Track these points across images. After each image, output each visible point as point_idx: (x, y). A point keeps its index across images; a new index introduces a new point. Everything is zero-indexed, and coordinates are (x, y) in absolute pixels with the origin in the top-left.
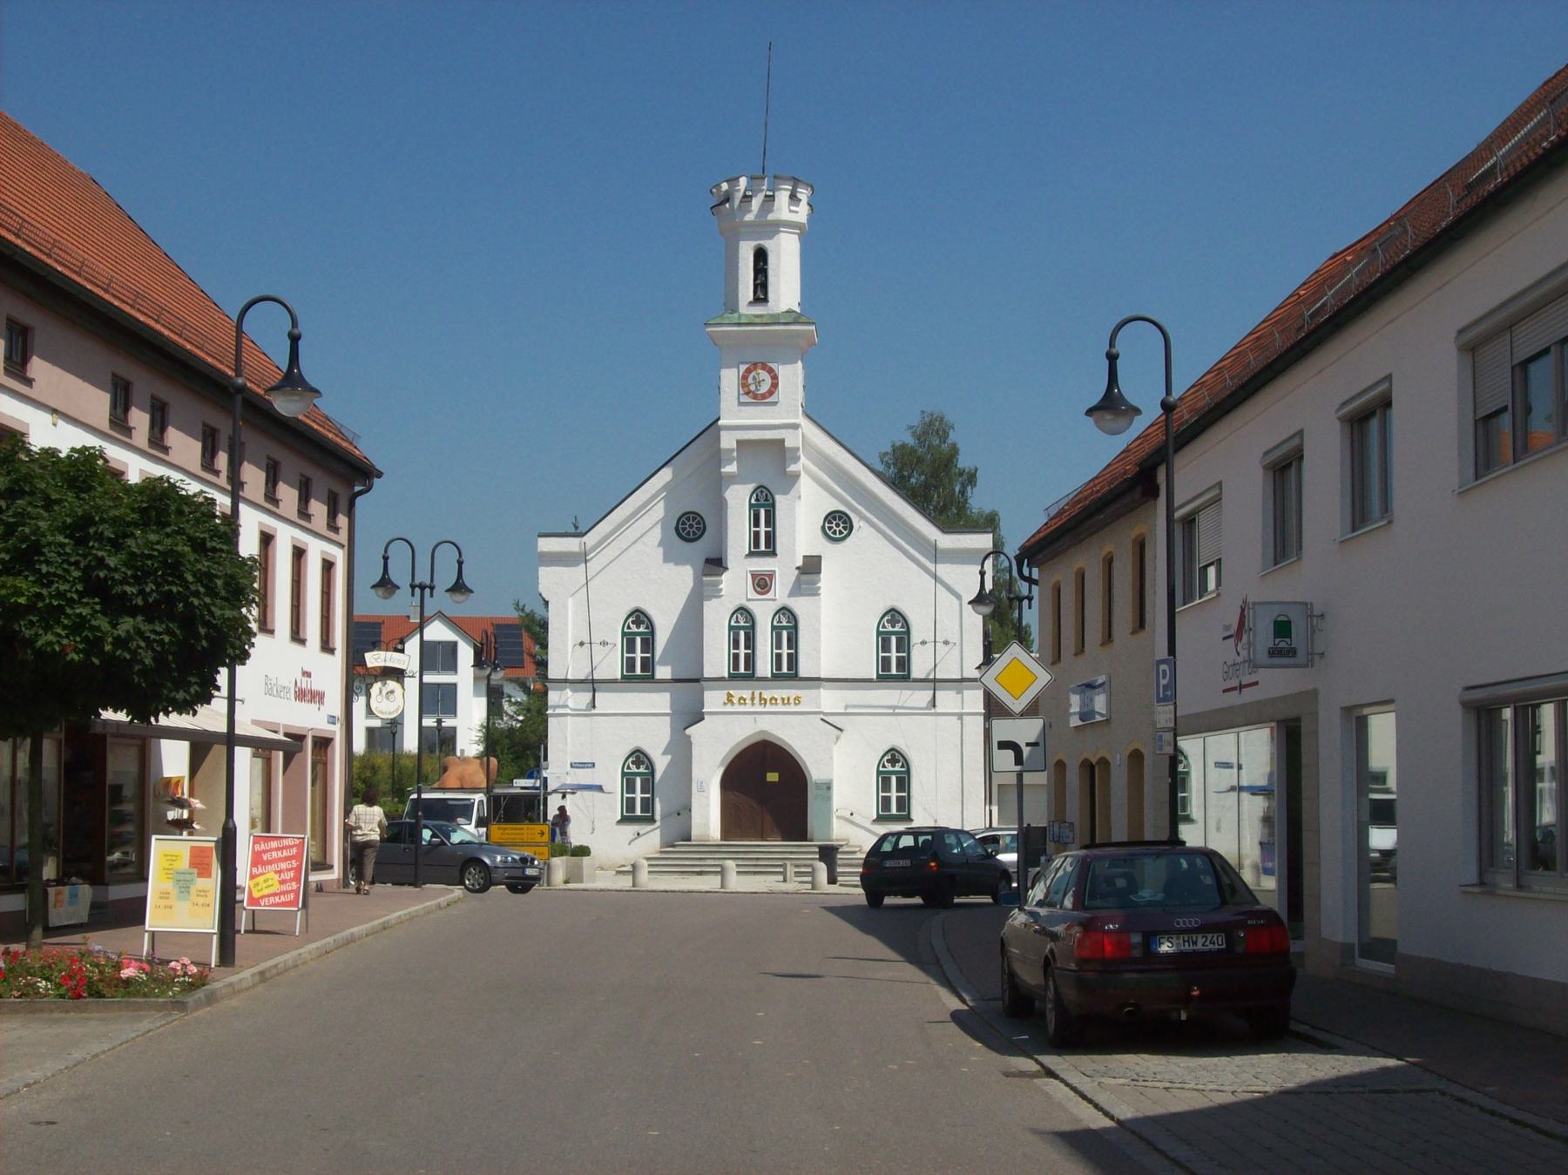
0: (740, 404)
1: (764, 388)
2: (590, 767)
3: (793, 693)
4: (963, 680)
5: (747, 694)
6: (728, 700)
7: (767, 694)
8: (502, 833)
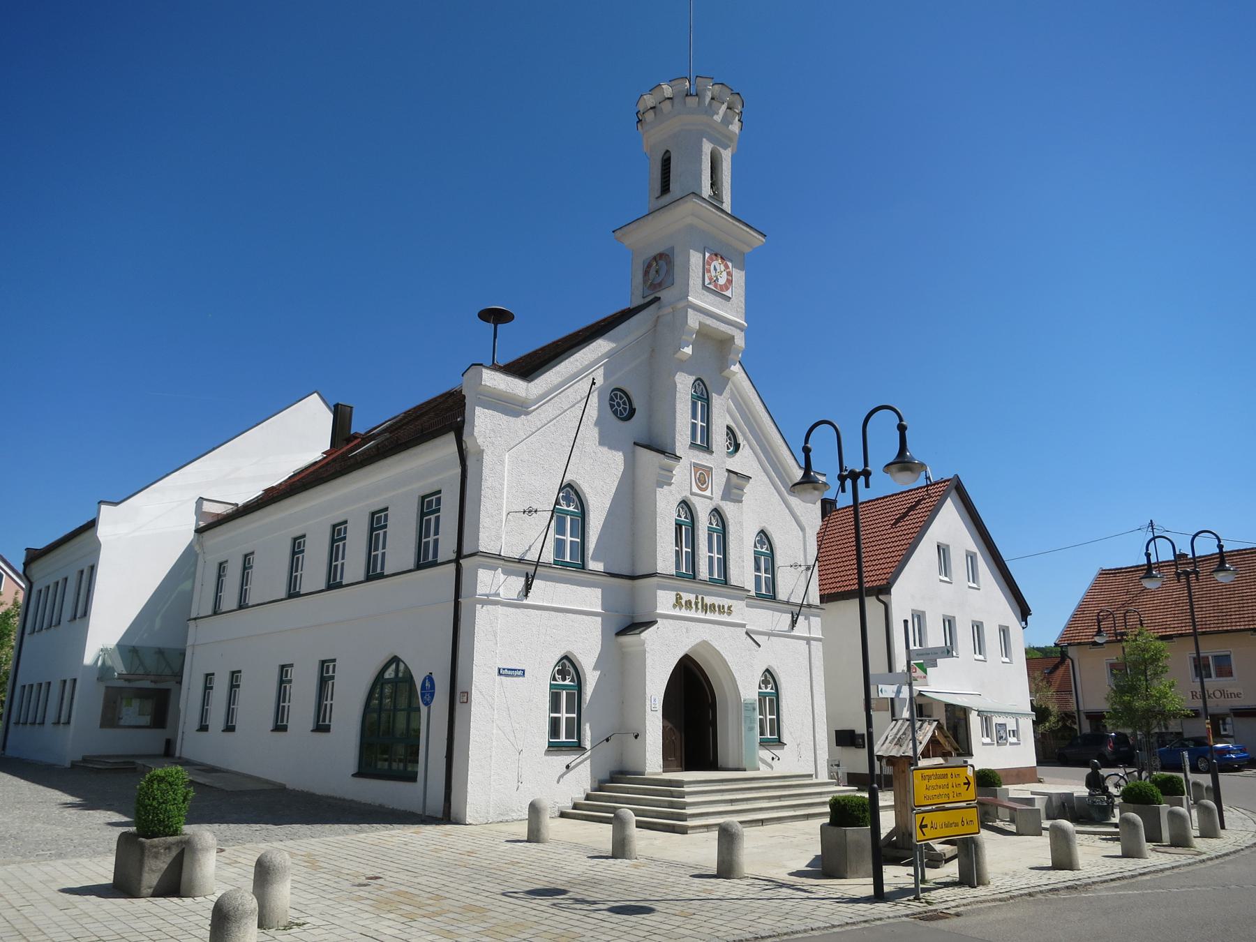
2: (520, 676)
3: (725, 602)
5: (692, 597)
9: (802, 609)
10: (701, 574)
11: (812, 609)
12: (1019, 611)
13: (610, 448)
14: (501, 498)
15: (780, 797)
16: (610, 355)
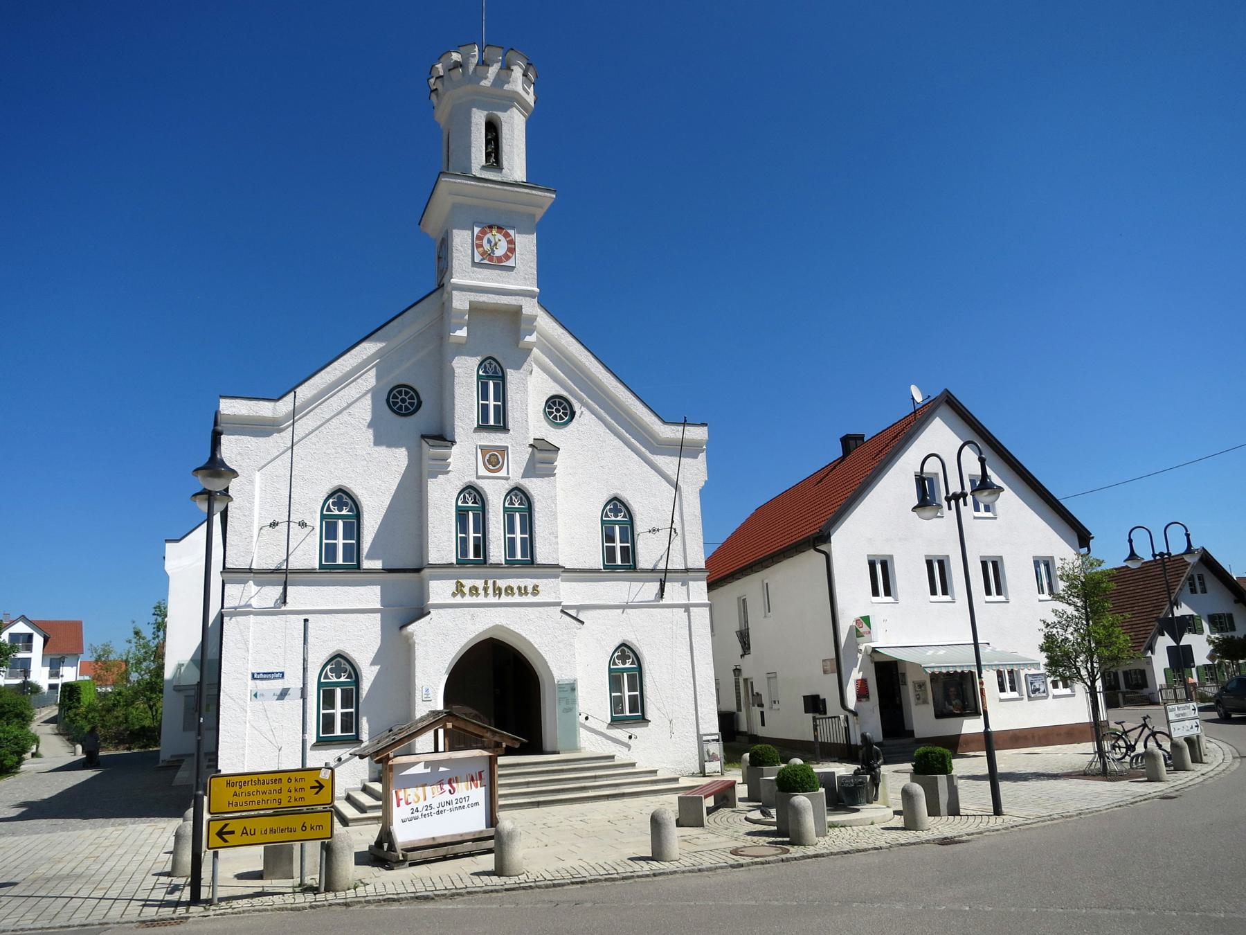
0: (474, 264)
1: (499, 252)
2: (279, 678)
3: (530, 583)
4: (687, 570)
5: (480, 583)
6: (457, 590)
7: (502, 584)
8: (235, 794)
9: (667, 574)
10: (491, 558)
11: (689, 574)
12: (1076, 534)
13: (389, 445)
14: (251, 515)
15: (527, 784)
16: (378, 354)
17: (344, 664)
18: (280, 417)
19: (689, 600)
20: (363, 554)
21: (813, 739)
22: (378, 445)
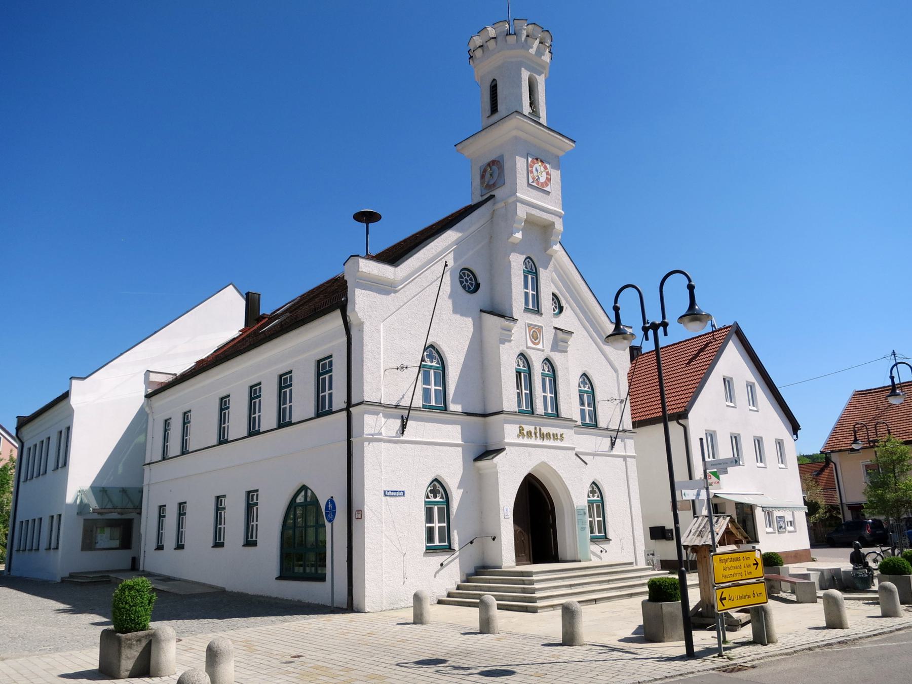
3: (558, 431)
5: (532, 429)
6: (520, 432)
9: (619, 433)
15: (608, 581)
16: (458, 242)
17: (438, 487)
18: (398, 281)
19: (626, 452)
20: (449, 399)
21: (676, 558)
22: (455, 313)
